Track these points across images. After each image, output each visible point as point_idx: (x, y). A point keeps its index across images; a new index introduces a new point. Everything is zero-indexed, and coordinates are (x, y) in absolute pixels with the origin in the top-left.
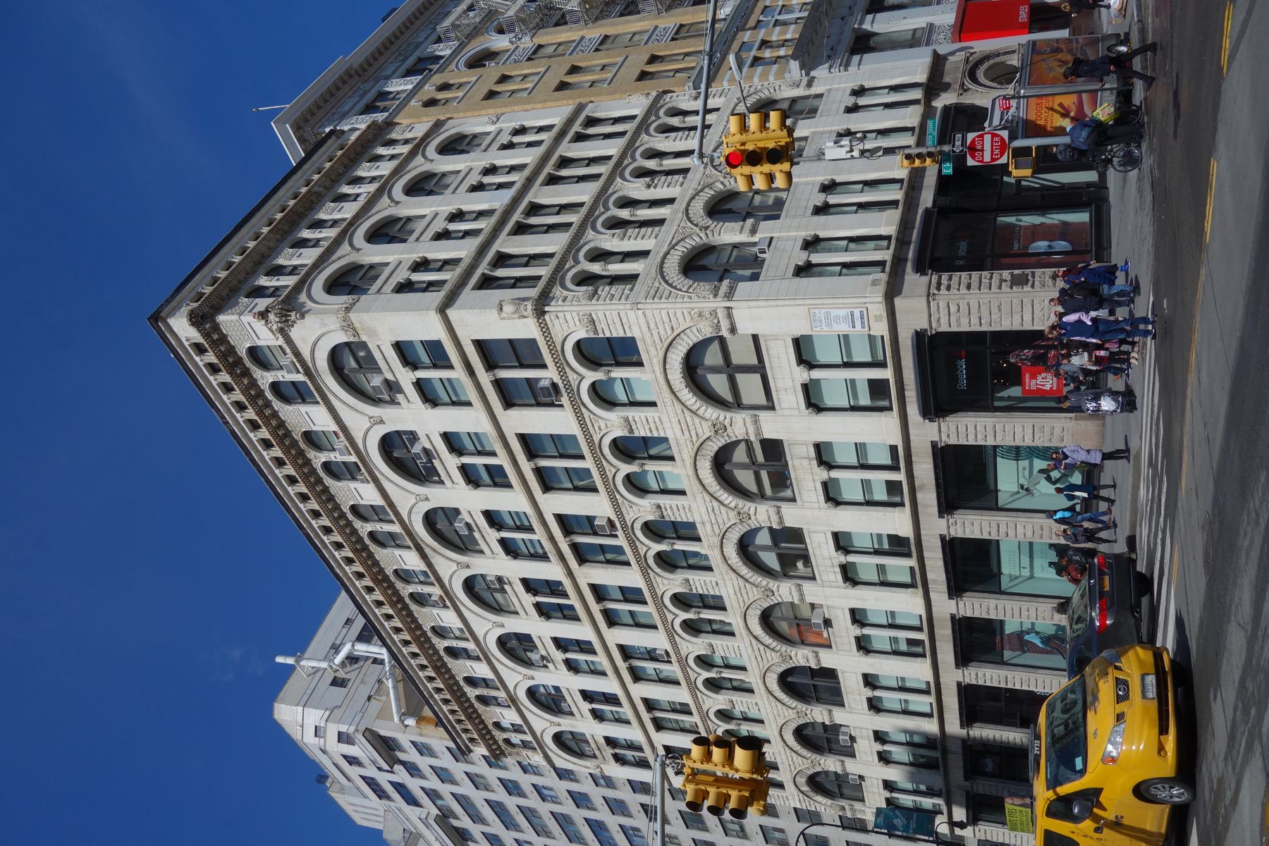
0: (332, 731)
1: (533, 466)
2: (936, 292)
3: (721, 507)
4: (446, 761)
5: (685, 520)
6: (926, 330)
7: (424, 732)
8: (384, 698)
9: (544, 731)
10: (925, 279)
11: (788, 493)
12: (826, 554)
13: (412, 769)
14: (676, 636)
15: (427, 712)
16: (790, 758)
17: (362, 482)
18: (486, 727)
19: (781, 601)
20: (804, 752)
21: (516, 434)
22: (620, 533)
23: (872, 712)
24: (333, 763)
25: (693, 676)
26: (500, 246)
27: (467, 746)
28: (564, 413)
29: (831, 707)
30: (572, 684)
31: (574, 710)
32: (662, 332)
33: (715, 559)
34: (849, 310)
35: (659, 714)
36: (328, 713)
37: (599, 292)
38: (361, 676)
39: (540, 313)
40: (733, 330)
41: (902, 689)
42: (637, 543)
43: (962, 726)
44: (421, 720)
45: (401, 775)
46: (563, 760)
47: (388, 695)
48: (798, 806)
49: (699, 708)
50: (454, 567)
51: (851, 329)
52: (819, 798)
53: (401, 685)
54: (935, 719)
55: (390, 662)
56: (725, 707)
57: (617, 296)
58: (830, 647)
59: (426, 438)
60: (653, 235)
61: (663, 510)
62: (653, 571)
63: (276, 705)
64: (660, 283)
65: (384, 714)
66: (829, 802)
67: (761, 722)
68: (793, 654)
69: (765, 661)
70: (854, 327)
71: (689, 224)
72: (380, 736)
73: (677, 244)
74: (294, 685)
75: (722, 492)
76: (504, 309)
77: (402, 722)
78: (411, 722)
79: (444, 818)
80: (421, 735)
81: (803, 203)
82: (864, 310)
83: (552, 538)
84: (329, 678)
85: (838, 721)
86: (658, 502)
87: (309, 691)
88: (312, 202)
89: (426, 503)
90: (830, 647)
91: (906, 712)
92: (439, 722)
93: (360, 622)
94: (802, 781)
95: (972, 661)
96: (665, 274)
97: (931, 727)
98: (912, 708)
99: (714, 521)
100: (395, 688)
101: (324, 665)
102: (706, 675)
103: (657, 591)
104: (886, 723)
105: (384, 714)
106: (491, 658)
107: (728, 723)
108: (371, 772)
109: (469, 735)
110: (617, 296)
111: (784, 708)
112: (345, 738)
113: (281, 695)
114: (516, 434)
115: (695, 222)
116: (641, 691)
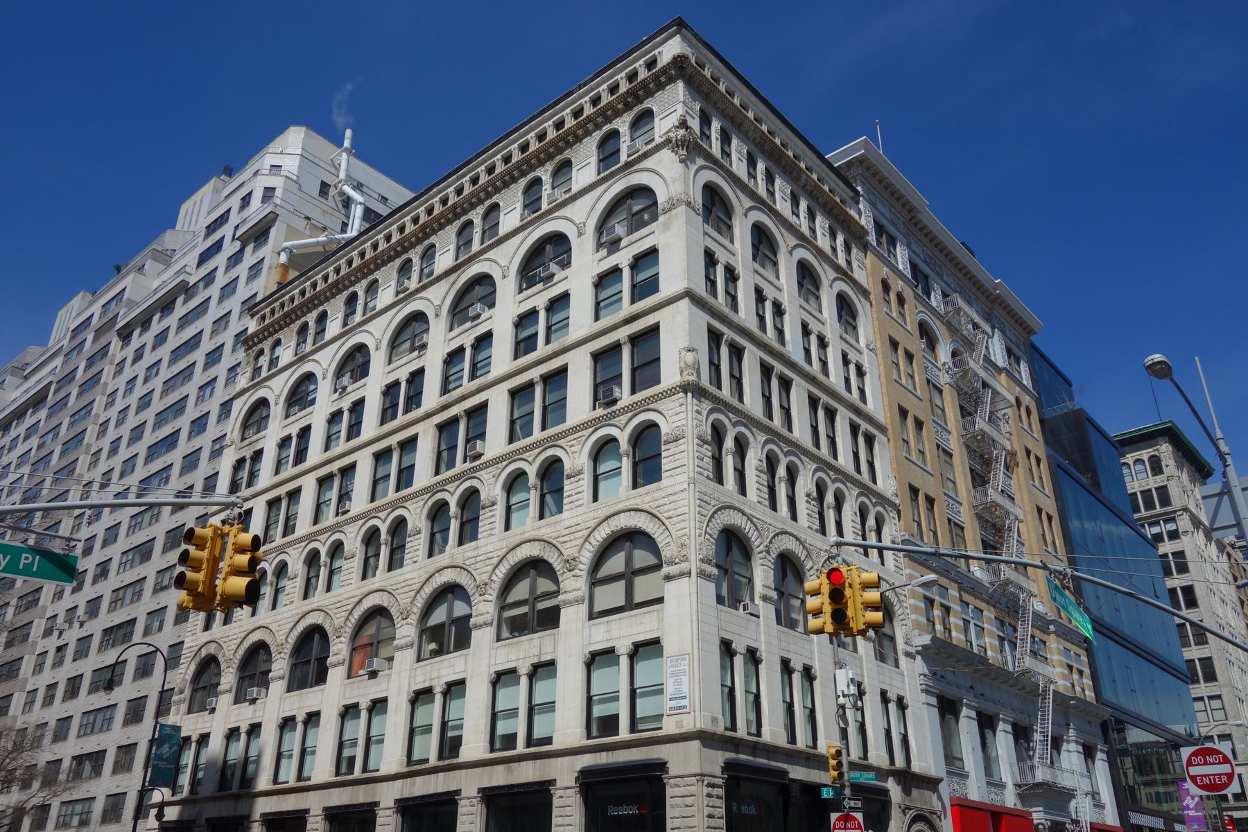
0: (276, 182)
1: (535, 380)
2: (705, 783)
3: (492, 566)
4: (243, 292)
5: (480, 530)
6: (667, 773)
7: (273, 272)
8: (308, 232)
9: (271, 389)
10: (718, 772)
11: (505, 634)
12: (444, 672)
13: (235, 259)
14: (363, 521)
15: (293, 274)
16: (235, 637)
17: (522, 215)
18: (276, 331)
19: (397, 627)
20: (241, 652)
21: (567, 364)
22: (468, 465)
23: (280, 721)
24: (244, 183)
25: (322, 538)
26: (749, 351)
27: (257, 313)
28: (588, 410)
29: (287, 678)
30: (317, 417)
31: (291, 419)
32: (666, 508)
33: (440, 560)
34: (687, 694)
35: (284, 504)
36: (294, 178)
37: (705, 446)
38: (331, 211)
39: (685, 388)
40: (668, 578)
41: (303, 752)
42: (458, 482)
43: (263, 815)
44: (285, 268)
45: (230, 248)
46: (240, 408)
47: (311, 237)
48: (185, 646)
49: (290, 544)
50: (437, 302)
51: (669, 697)
52: (193, 667)
53: (320, 249)
54: (271, 787)
55: (343, 239)
56: (290, 570)
57: (701, 464)
58: (349, 677)
59: (564, 277)
60: (761, 500)
61: (490, 508)
62: (429, 498)
63: (303, 129)
64: (714, 506)
65: (292, 232)
66: (189, 678)
67: (274, 607)
68: (342, 639)
69: (336, 611)
70: (671, 699)
71: (771, 535)
72: (270, 228)
73: (752, 522)
74: (322, 146)
75: (508, 567)
76: (690, 353)
77: (284, 250)
78: (283, 258)
79: (186, 290)
80: (270, 268)
81: (792, 648)
82: (687, 710)
83: (464, 398)
84: (329, 179)
85: (272, 685)
86: (499, 503)
87: (316, 161)
88: (791, 173)
89: (500, 276)
90: (349, 677)
91: (279, 756)
92: (282, 286)
93: (383, 210)
94: (212, 649)
95: (488, 807)
96: (723, 511)
97: (264, 782)
98: (284, 762)
99: (478, 559)
100: (318, 243)
101: (342, 175)
102: (323, 551)
103: (409, 502)
104: (269, 735)
105: (292, 232)
106: (345, 338)
107: (327, 554)
108: (234, 219)
109: (268, 315)
110: (701, 464)
111: (288, 631)
112: (269, 194)
113: (314, 134)
114: (567, 364)
115: (773, 541)
116: (309, 485)
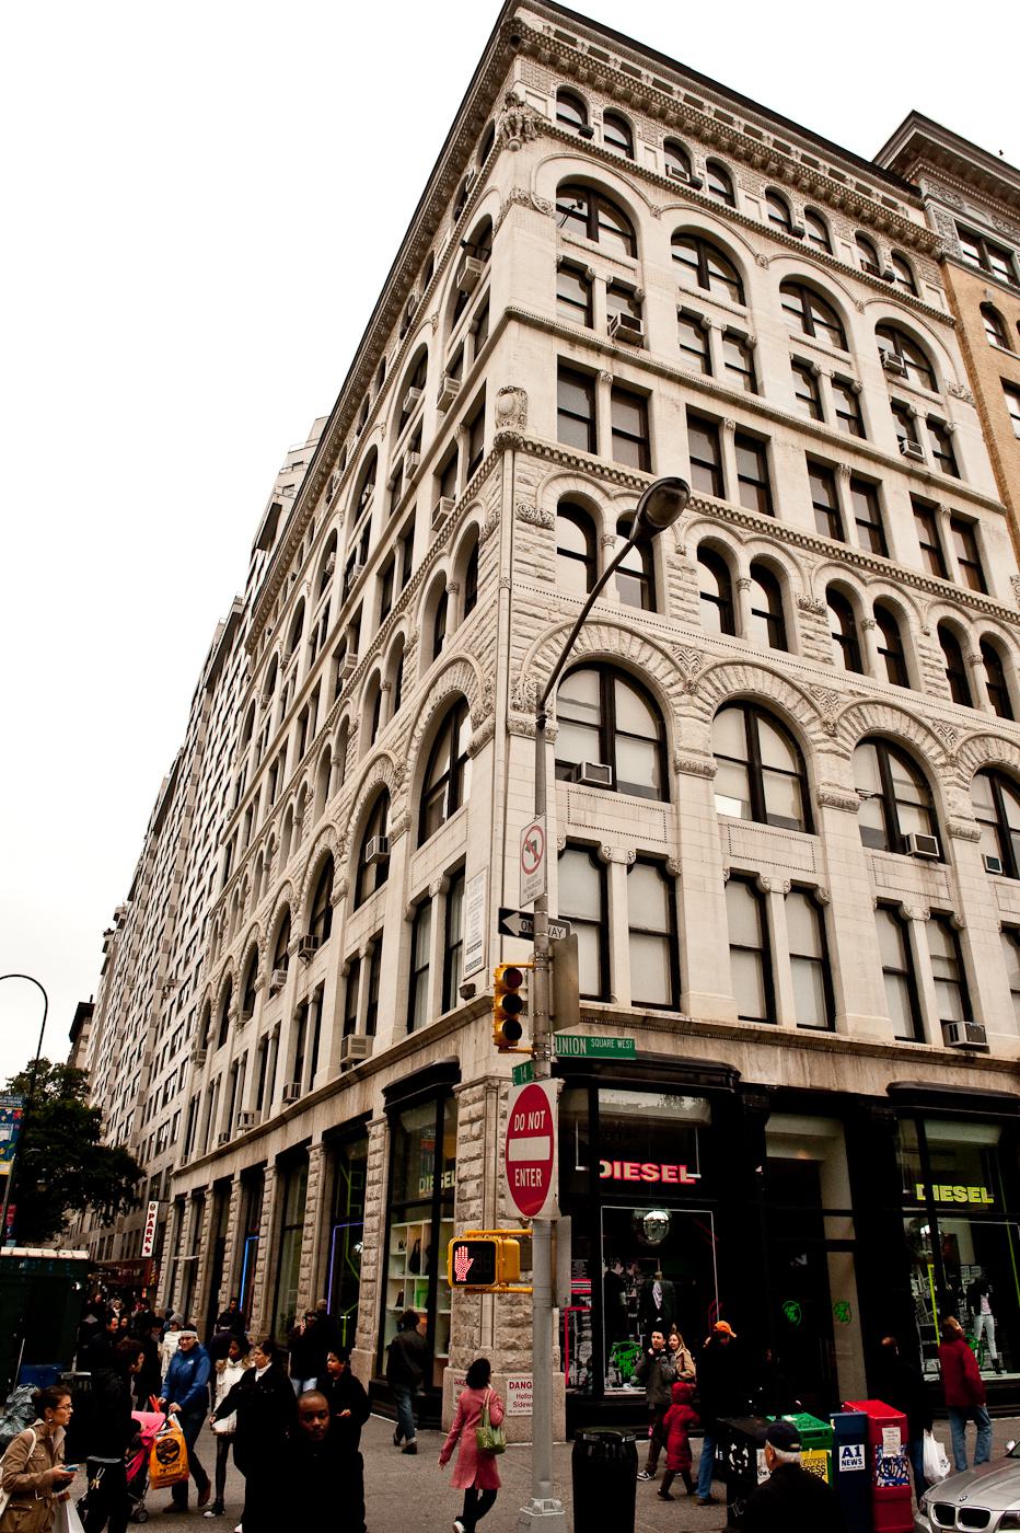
98: (810, 948)
